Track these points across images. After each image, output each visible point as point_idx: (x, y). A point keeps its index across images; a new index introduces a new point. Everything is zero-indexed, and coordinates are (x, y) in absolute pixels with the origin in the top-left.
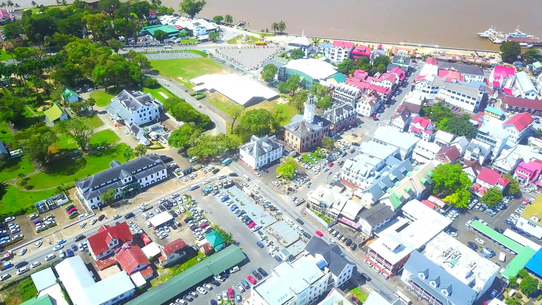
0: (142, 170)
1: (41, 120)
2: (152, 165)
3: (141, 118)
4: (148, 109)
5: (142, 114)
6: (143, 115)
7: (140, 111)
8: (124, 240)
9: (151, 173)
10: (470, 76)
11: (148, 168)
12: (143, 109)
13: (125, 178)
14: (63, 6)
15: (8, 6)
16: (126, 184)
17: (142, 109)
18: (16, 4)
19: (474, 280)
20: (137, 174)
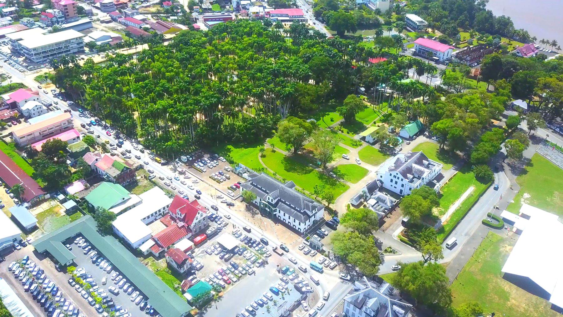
0: (289, 206)
1: (256, 115)
2: (299, 209)
3: (391, 184)
4: (402, 180)
5: (394, 180)
6: (394, 182)
7: (393, 176)
8: (186, 221)
9: (290, 214)
10: (182, 196)
11: (294, 209)
12: (397, 176)
13: (270, 198)
14: (478, 66)
15: (550, 45)
16: (268, 202)
17: (395, 175)
18: (559, 47)
19: (7, 129)
20: (283, 204)
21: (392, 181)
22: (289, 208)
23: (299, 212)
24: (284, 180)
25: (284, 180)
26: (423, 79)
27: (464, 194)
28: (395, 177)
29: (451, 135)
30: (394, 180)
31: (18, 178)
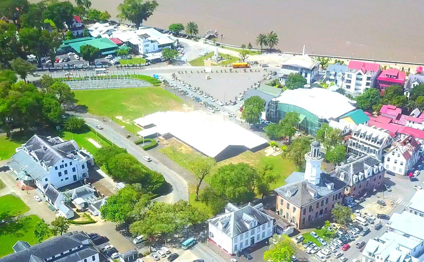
0: (63, 256)
2: (77, 248)
3: (61, 178)
4: (71, 164)
5: (62, 171)
6: (63, 173)
7: (59, 167)
11: (71, 252)
12: (64, 163)
17: (61, 164)
21: (60, 174)
22: (64, 258)
23: (79, 249)
24: (256, 89)
25: (256, 89)
26: (30, 78)
27: (96, 146)
28: (62, 167)
29: (25, 108)
30: (62, 171)
31: (304, 48)
